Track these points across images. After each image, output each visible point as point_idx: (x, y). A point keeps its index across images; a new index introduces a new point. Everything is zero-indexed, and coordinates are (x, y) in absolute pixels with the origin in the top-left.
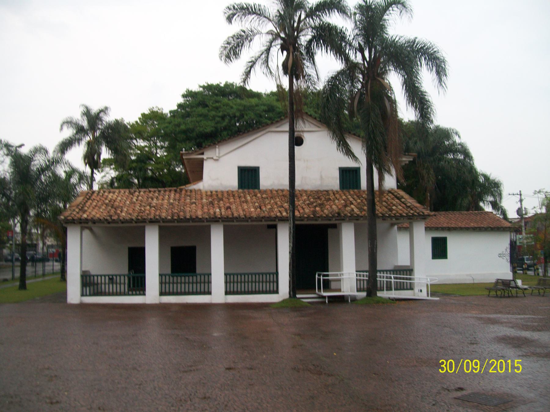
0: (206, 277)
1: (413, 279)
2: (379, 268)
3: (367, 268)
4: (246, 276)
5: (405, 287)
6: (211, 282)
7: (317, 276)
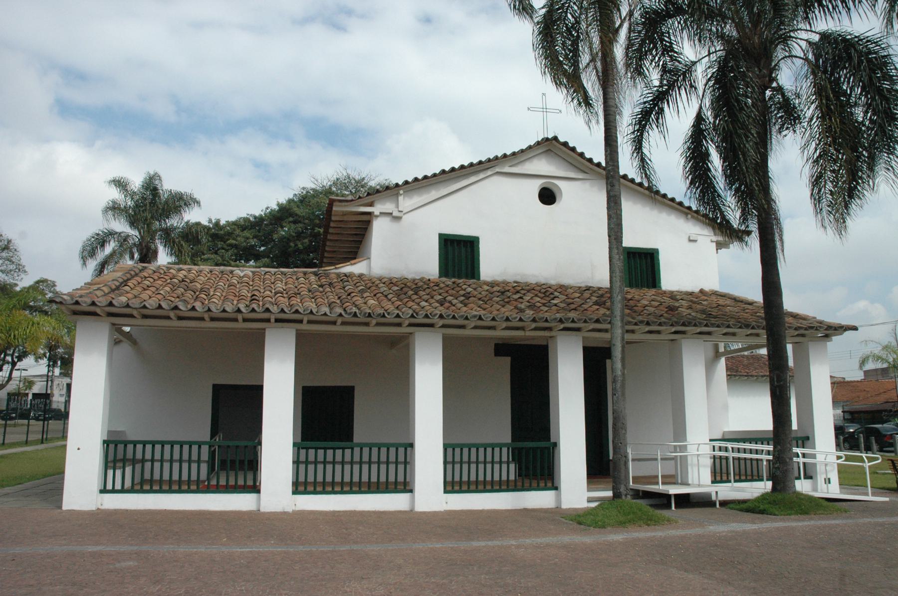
0: (401, 450)
4: (466, 451)
6: (294, 462)
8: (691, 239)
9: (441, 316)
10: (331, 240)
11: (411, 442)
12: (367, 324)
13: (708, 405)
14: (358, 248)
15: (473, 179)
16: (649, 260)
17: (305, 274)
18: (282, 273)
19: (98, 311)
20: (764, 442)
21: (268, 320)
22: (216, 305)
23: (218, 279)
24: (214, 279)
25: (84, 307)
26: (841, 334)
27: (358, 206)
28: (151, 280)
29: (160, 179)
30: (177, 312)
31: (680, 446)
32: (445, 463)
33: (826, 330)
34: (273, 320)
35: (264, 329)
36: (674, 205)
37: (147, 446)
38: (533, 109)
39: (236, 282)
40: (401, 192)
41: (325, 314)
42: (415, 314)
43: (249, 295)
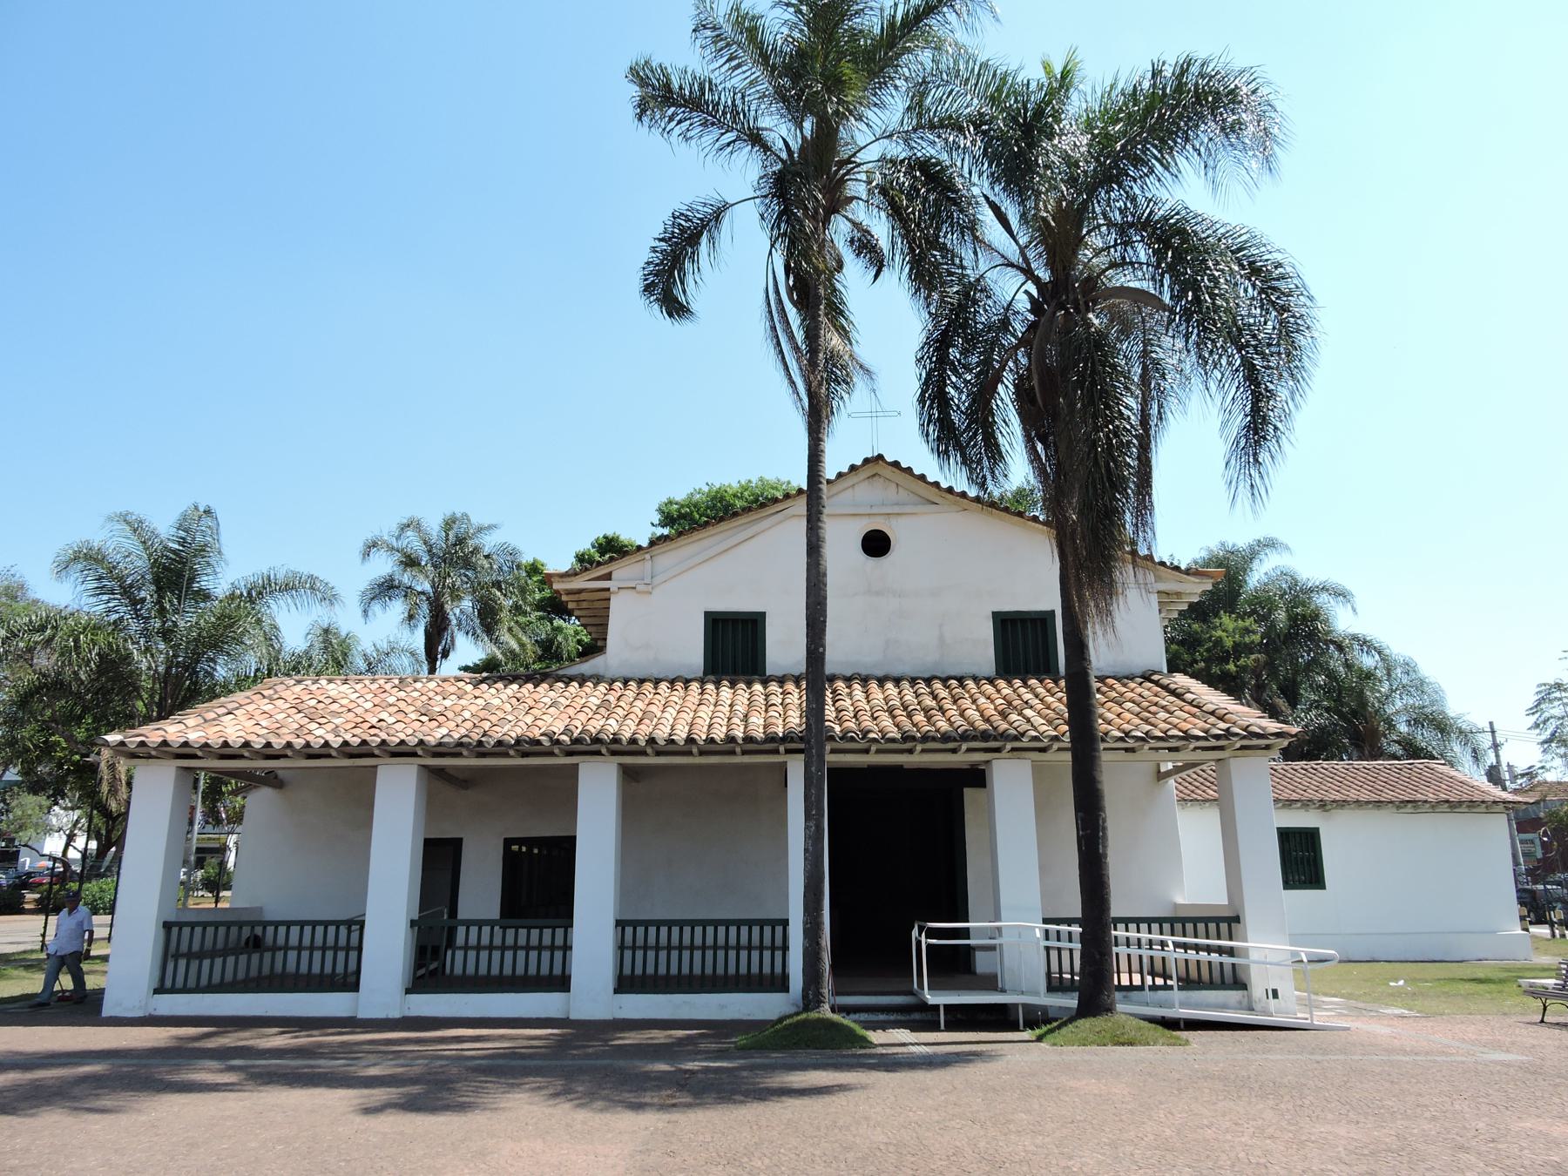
1: (1244, 953)
2: (1116, 911)
3: (1075, 909)
5: (1297, 835)
6: (571, 948)
7: (915, 933)
11: (785, 917)
13: (1043, 869)
29: (670, 502)
32: (360, 949)
35: (376, 767)
37: (317, 928)
38: (857, 415)
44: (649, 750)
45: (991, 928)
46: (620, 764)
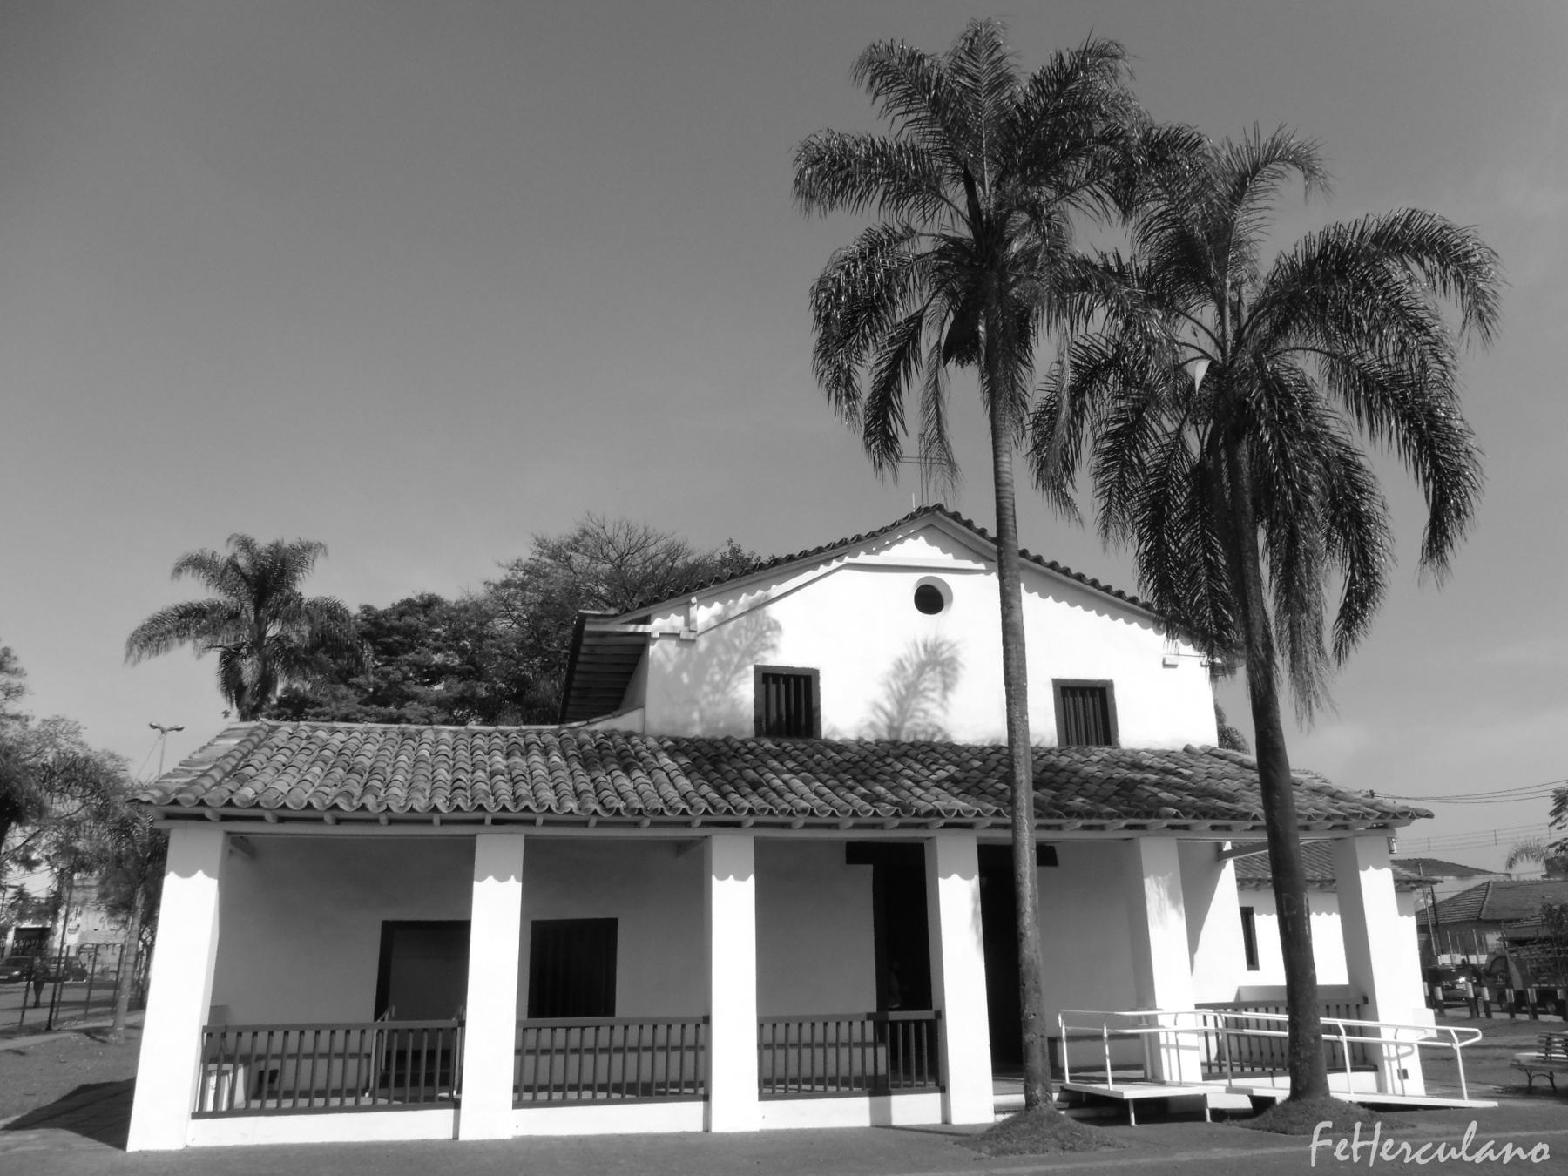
8: (1167, 662)
9: (751, 812)
10: (580, 672)
12: (636, 825)
14: (627, 683)
15: (809, 575)
16: (1098, 699)
17: (539, 734)
18: (501, 733)
19: (208, 813)
20: (1270, 1009)
21: (481, 822)
22: (397, 797)
23: (396, 748)
24: (390, 748)
25: (186, 808)
26: (1408, 824)
27: (626, 623)
28: (288, 752)
30: (336, 813)
31: (1147, 1017)
33: (1379, 818)
34: (488, 821)
35: (475, 835)
36: (1137, 607)
39: (427, 754)
40: (694, 600)
41: (571, 812)
42: (710, 810)
43: (449, 778)
44: (328, 817)
45: (1133, 1016)
46: (229, 833)
